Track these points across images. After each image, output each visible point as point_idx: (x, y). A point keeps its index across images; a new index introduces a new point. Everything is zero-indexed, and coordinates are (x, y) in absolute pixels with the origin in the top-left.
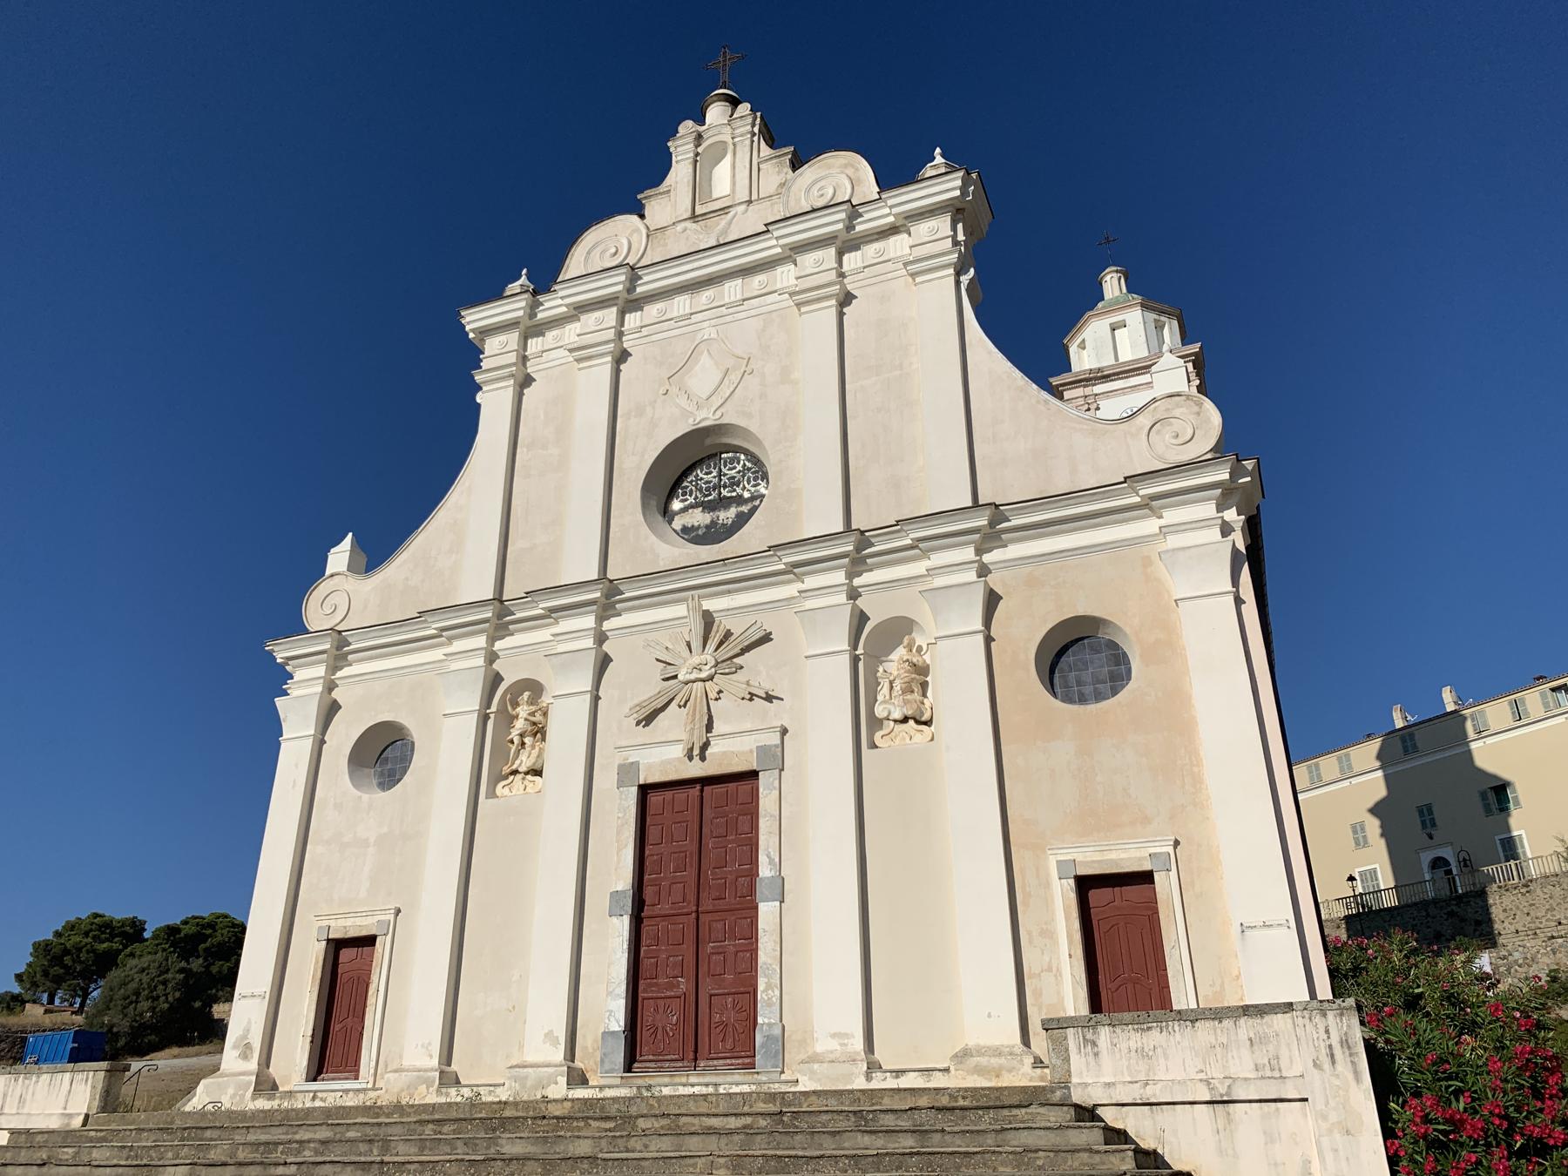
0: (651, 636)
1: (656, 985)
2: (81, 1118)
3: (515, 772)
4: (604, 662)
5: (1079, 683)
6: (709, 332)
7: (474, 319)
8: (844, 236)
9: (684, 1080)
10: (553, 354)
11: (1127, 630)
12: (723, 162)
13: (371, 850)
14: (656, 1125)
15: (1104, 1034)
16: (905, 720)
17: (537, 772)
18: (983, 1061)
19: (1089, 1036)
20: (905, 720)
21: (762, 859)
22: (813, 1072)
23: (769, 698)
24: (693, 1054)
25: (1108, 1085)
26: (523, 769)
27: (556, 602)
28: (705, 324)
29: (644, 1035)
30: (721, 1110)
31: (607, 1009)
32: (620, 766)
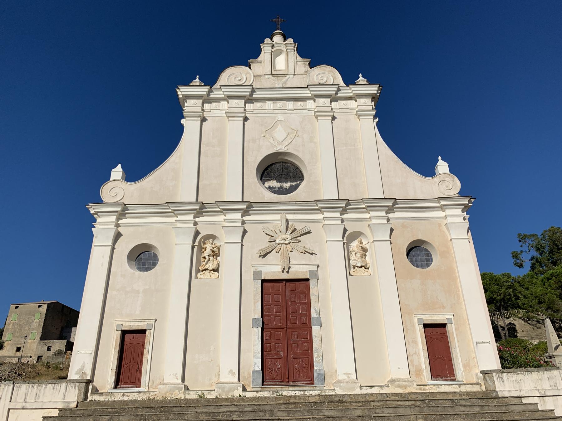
0: (265, 225)
1: (271, 354)
2: (76, 403)
3: (207, 269)
4: (245, 232)
5: (416, 261)
6: (280, 118)
7: (182, 91)
8: (206, 97)
9: (287, 389)
10: (215, 112)
11: (435, 246)
12: (279, 57)
13: (141, 295)
14: (378, 404)
15: (505, 375)
16: (361, 267)
17: (216, 270)
18: (400, 383)
19: (500, 376)
20: (361, 267)
21: (313, 310)
22: (340, 387)
23: (312, 254)
24: (287, 379)
25: (509, 391)
26: (210, 268)
27: (224, 207)
28: (279, 115)
29: (266, 372)
30: (379, 399)
31: (254, 361)
32: (254, 272)
